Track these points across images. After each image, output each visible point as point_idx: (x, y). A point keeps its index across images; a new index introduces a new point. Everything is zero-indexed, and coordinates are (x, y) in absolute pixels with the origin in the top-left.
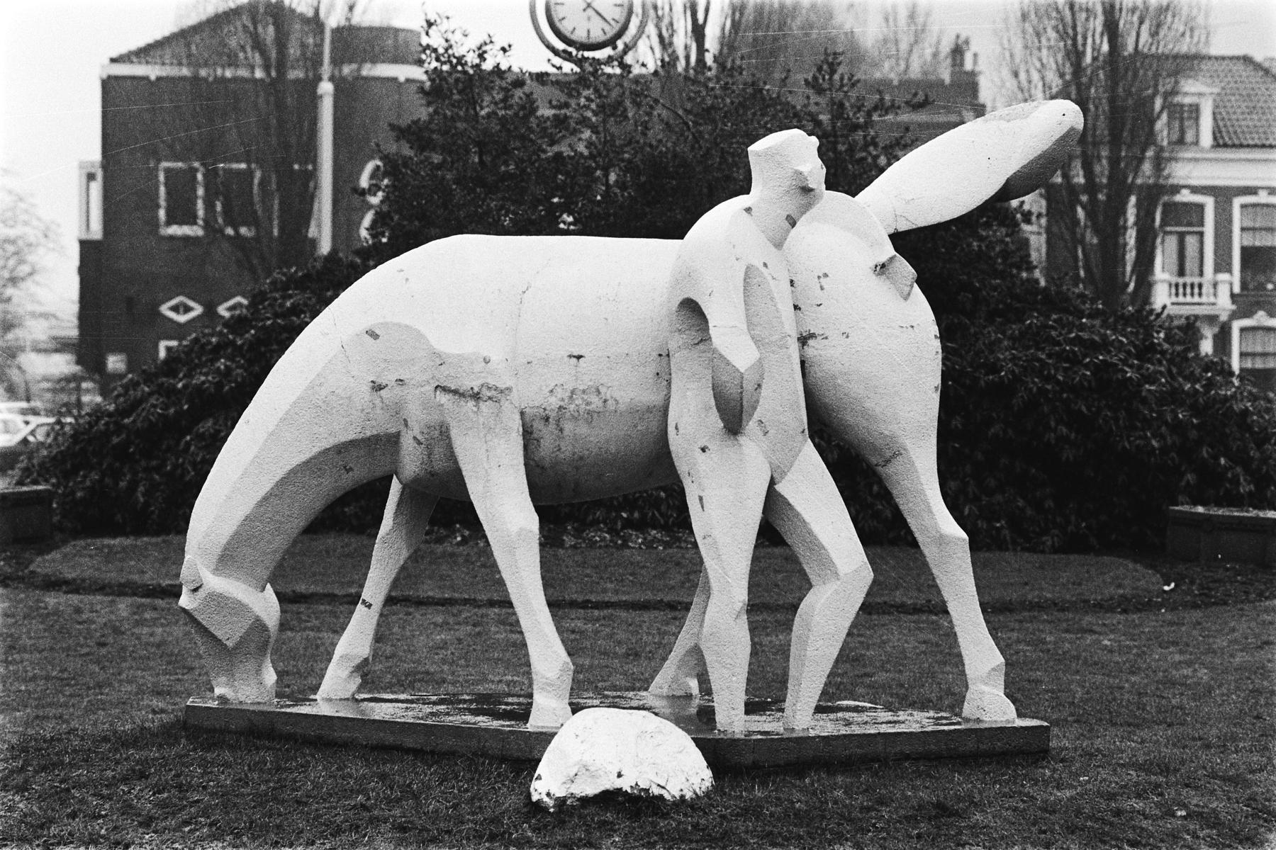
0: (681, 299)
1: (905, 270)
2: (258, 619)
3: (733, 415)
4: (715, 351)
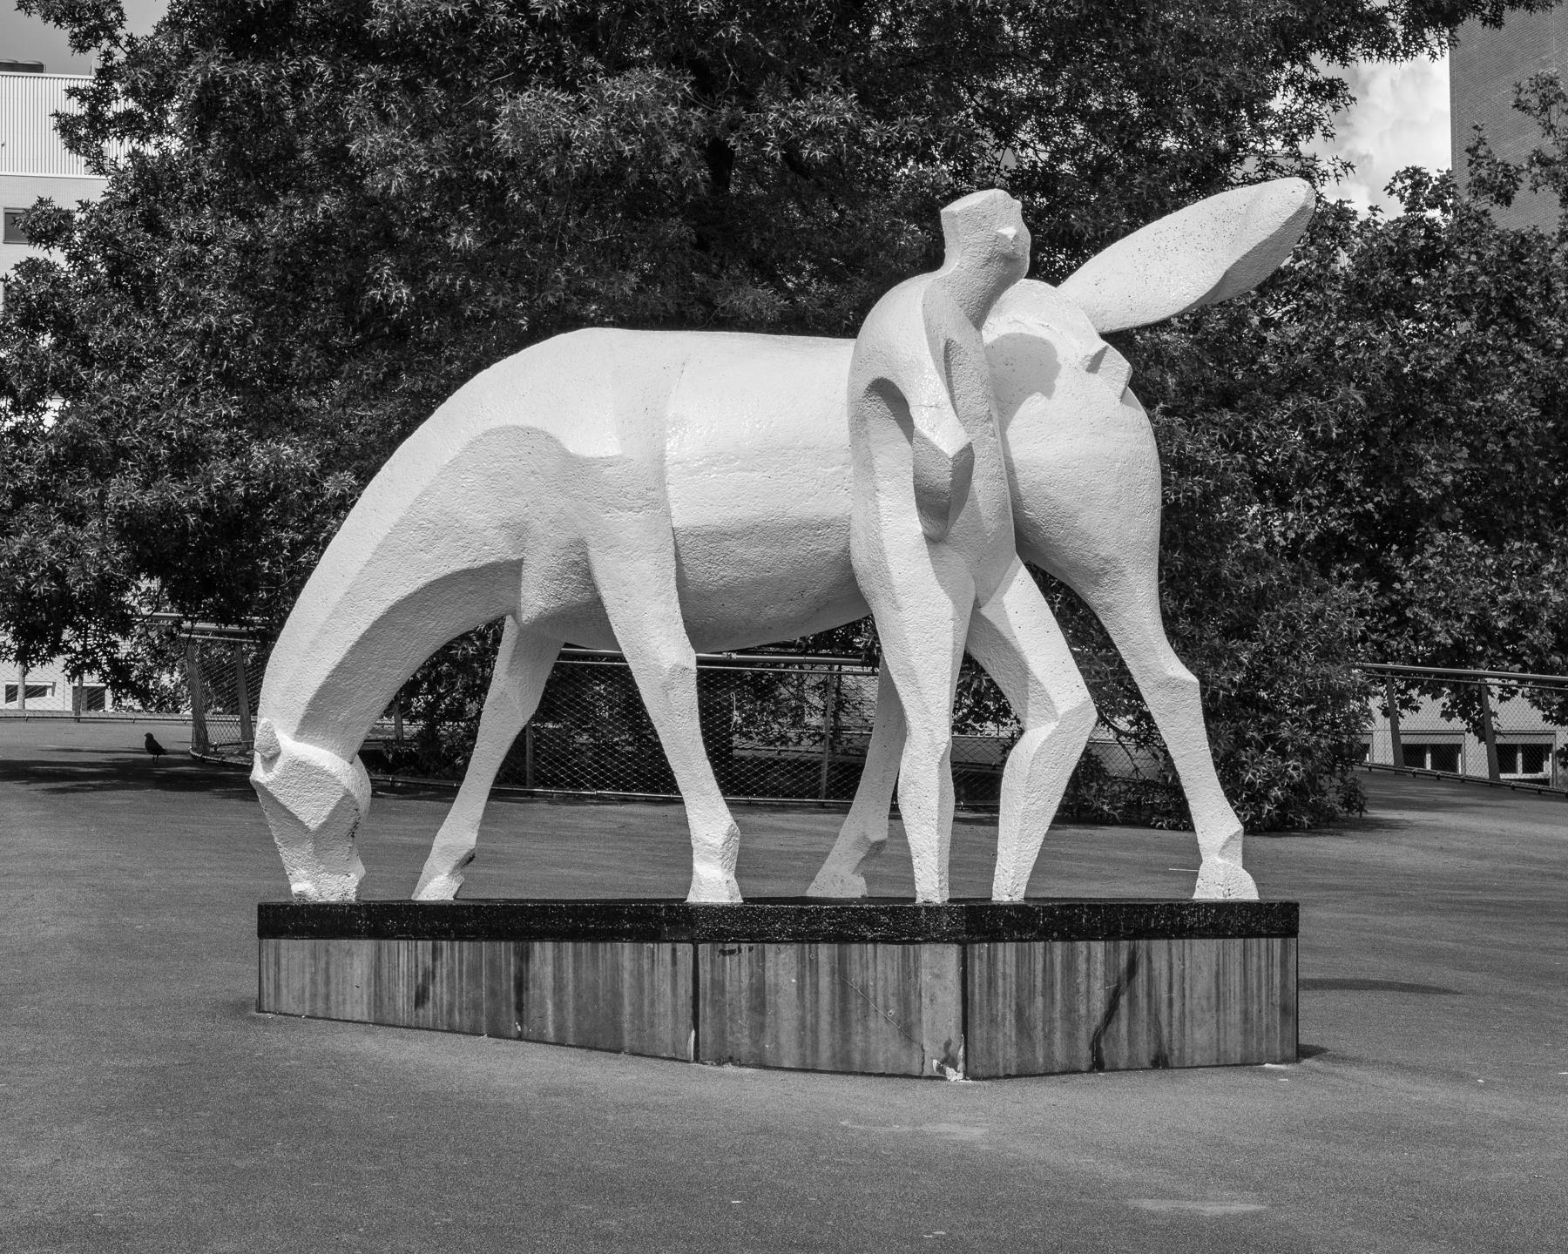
1: (1119, 367)
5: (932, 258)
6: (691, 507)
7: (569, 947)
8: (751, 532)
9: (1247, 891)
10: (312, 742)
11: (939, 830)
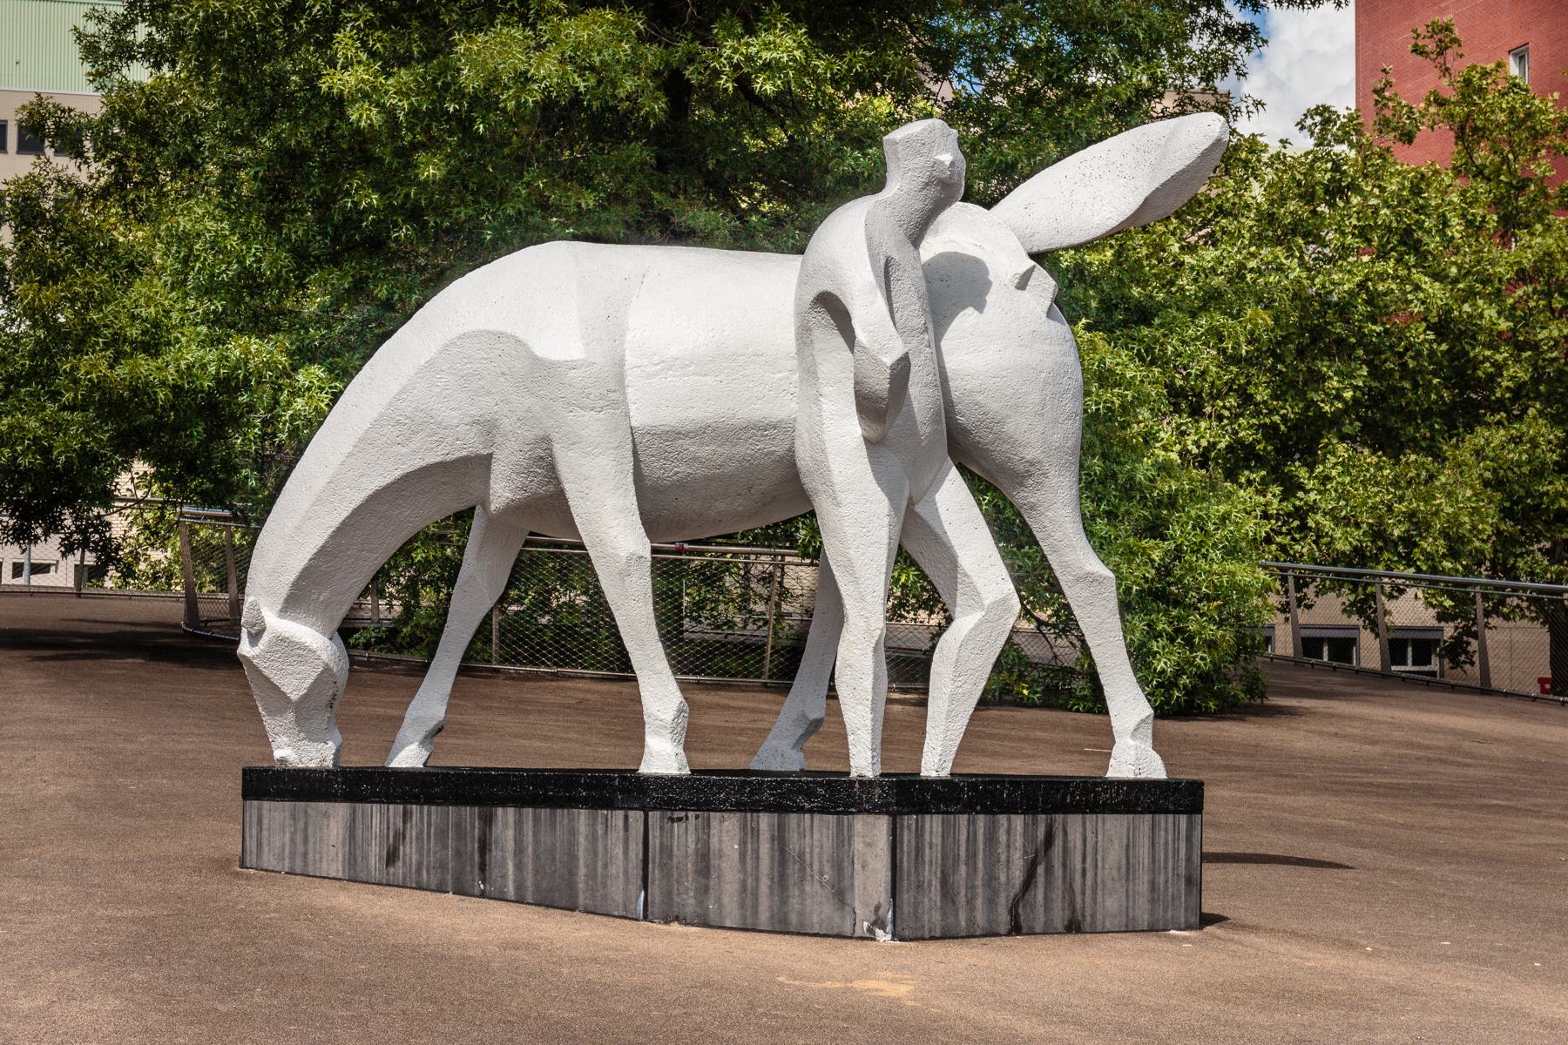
5: (873, 181)
8: (702, 433)
9: (1156, 770)
10: (295, 619)
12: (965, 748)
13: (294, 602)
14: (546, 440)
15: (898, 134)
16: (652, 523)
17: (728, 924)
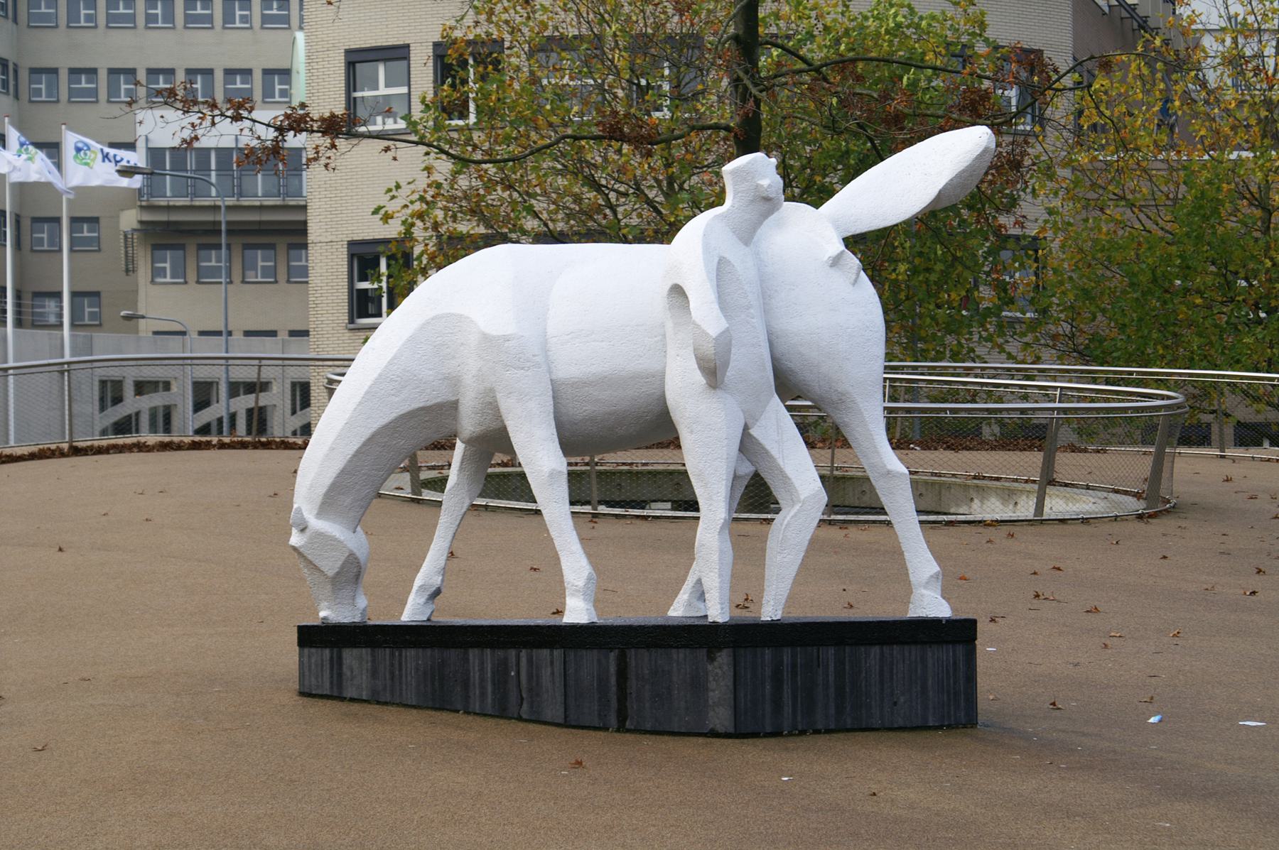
0: (667, 287)
1: (853, 261)
2: (352, 554)
3: (713, 372)
4: (694, 323)
5: (719, 200)
6: (577, 361)
7: (906, 647)
8: (603, 381)
9: (942, 610)
10: (328, 519)
11: (721, 576)
12: (791, 599)
13: (330, 503)
14: (492, 390)
15: (728, 168)
16: (569, 445)
17: (549, 719)
